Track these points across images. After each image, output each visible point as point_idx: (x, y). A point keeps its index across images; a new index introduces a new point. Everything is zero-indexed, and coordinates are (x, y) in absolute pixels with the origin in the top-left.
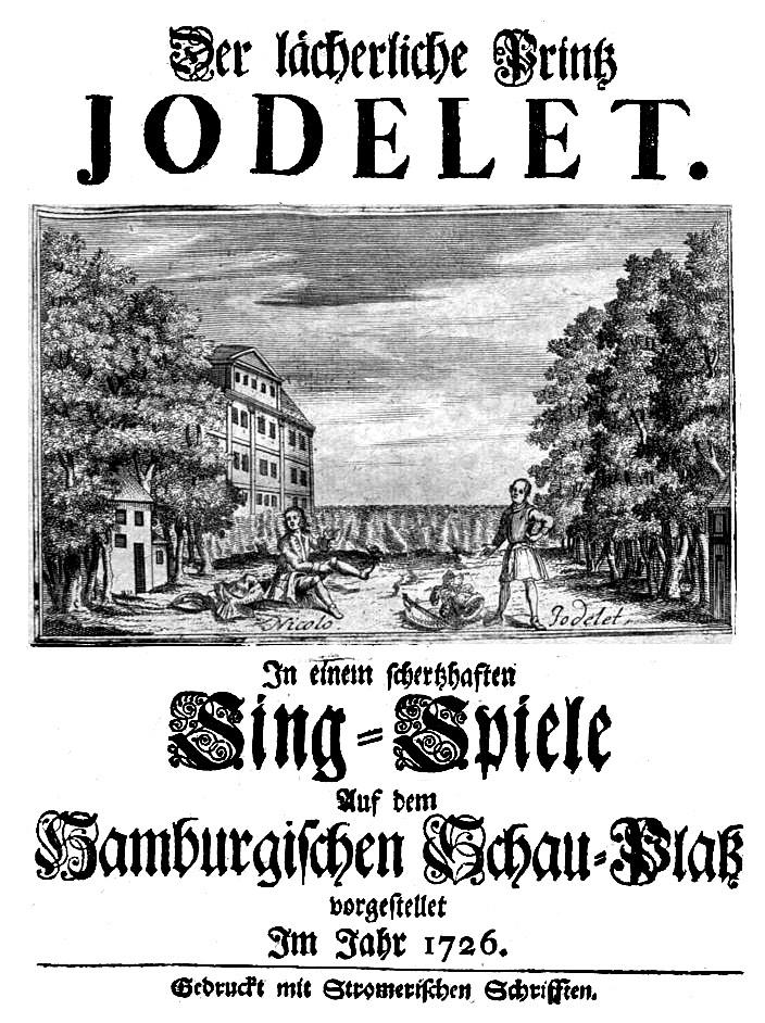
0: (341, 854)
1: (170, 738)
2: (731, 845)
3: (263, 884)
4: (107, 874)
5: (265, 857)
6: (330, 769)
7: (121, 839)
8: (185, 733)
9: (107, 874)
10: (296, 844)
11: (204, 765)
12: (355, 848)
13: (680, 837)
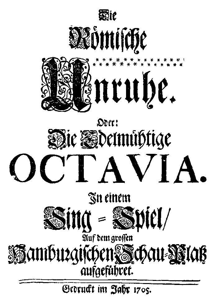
0: (143, 254)
1: (44, 220)
2: (203, 251)
3: (74, 264)
4: (193, 262)
5: (74, 257)
6: (87, 229)
7: (33, 250)
8: (117, 219)
9: (193, 262)
10: (83, 252)
11: (55, 228)
12: (100, 253)
13: (188, 249)
